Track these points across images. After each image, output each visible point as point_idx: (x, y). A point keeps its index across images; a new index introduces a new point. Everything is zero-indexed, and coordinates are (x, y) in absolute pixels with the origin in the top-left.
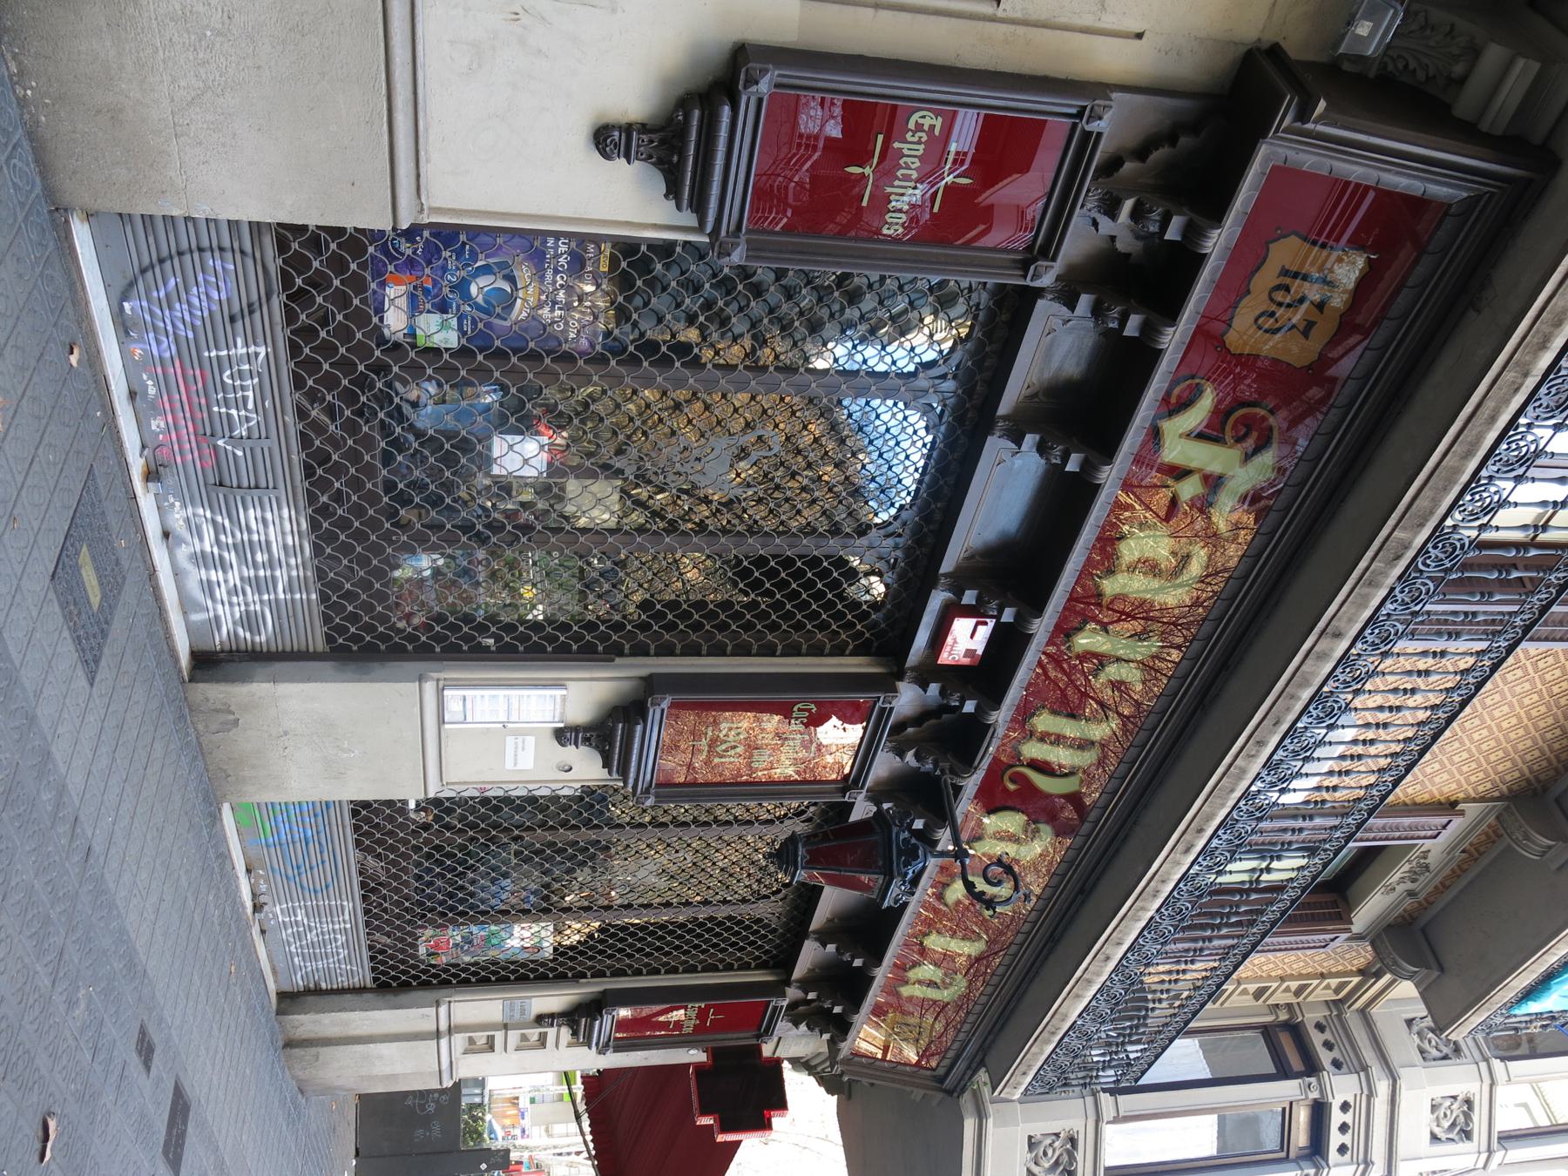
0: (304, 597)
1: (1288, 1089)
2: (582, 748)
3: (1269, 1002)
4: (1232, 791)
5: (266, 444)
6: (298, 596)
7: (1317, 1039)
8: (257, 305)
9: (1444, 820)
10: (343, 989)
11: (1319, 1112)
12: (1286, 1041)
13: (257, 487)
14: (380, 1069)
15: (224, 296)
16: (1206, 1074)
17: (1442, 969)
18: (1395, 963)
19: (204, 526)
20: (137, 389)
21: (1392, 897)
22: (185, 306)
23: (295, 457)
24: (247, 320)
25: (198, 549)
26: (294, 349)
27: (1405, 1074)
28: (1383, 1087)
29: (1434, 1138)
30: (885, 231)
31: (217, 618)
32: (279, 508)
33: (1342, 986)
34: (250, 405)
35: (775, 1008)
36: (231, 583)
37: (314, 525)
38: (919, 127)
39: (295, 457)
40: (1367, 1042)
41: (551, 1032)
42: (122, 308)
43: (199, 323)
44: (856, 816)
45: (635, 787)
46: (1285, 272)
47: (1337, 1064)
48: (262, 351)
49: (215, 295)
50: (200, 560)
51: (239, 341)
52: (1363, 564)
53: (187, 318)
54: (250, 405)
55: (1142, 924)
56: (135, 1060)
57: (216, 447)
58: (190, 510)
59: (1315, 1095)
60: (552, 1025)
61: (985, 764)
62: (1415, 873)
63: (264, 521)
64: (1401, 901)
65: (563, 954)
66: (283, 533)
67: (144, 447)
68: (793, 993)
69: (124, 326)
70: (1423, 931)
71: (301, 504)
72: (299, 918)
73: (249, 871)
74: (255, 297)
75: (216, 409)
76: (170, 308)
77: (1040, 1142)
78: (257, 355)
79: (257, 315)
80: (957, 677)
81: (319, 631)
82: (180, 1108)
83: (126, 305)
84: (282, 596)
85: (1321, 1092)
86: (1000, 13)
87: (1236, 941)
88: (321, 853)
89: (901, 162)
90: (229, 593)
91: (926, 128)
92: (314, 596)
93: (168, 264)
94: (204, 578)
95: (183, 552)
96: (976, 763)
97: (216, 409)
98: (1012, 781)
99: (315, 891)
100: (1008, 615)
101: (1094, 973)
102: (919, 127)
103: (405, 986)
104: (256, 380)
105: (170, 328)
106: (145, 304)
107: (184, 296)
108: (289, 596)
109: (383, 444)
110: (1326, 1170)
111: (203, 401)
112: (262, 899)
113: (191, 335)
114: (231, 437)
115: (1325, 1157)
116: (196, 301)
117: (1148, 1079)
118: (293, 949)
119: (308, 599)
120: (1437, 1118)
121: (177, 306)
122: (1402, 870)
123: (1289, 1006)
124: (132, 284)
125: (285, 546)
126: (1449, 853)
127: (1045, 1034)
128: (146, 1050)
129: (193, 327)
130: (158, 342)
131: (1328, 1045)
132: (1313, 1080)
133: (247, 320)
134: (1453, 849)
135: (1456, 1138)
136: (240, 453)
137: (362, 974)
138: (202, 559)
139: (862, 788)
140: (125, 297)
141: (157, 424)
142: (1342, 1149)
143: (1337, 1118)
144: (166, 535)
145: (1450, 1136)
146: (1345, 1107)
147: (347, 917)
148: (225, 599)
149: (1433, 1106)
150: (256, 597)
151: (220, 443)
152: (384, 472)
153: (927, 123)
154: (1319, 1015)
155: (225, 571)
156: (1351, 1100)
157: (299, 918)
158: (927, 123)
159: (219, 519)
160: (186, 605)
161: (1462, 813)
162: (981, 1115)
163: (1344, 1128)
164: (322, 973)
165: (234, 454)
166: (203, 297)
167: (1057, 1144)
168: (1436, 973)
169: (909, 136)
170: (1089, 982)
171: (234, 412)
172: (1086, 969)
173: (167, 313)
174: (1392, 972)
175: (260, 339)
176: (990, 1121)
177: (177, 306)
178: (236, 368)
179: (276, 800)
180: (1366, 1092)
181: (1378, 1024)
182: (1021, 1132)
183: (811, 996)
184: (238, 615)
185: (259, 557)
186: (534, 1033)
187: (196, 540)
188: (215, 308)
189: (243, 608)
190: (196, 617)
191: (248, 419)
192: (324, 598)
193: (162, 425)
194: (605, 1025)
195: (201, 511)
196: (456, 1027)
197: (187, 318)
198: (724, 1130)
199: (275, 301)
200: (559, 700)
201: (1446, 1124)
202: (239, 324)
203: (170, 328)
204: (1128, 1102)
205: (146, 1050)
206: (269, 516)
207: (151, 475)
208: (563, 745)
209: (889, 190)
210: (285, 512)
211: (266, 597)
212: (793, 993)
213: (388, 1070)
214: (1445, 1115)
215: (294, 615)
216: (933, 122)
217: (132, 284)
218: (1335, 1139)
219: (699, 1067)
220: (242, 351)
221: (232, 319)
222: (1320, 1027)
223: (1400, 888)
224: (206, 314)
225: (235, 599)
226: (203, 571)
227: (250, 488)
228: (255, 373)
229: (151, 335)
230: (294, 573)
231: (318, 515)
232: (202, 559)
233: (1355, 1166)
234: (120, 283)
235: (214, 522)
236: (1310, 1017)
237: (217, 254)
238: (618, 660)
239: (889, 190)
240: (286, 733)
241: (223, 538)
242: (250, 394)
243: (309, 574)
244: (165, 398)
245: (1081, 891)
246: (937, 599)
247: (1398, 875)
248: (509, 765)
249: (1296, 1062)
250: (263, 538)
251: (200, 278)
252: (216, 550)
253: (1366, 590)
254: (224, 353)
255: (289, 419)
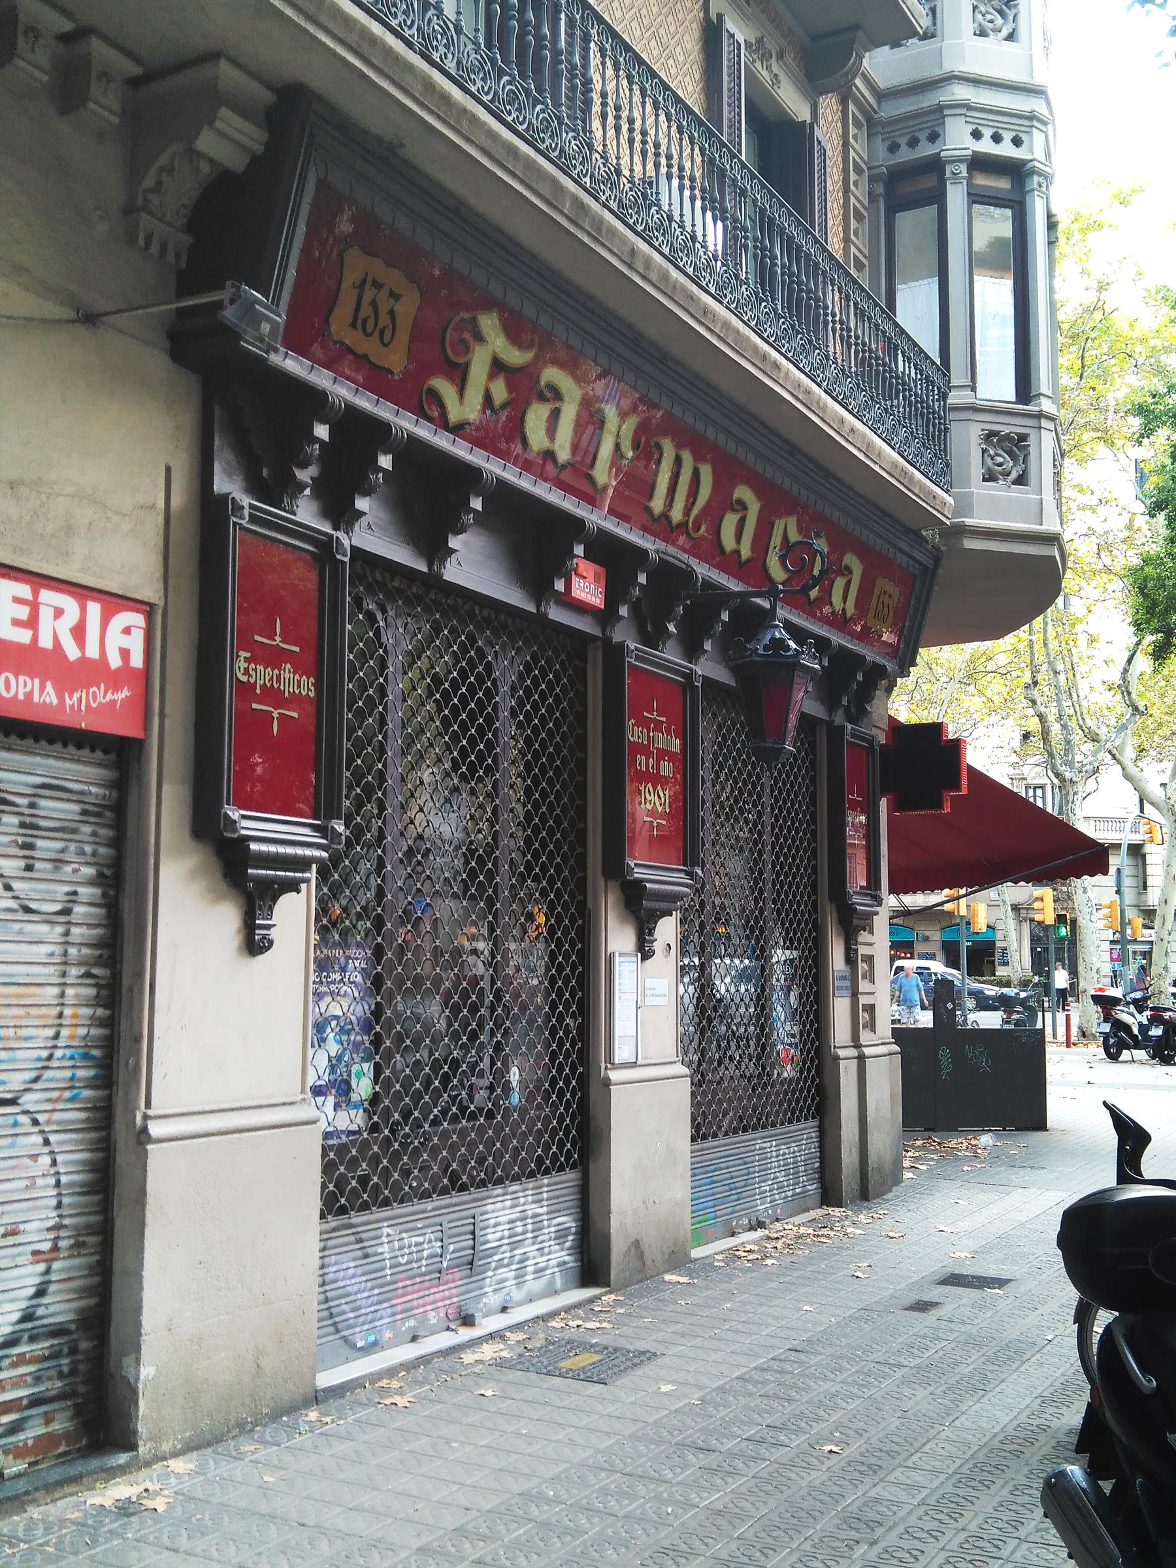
0: (545, 1189)
1: (956, 196)
2: (656, 936)
3: (866, 203)
4: (738, 332)
5: (446, 1226)
6: (545, 1195)
7: (905, 155)
8: (358, 1236)
9: (725, 35)
10: (820, 1147)
11: (979, 163)
12: (905, 188)
13: (473, 1233)
14: (886, 1111)
15: (352, 1264)
16: (933, 284)
17: (856, 27)
18: (846, 74)
19: (498, 1277)
20: (410, 1336)
21: (783, 78)
22: (359, 1296)
23: (455, 1200)
24: (366, 1244)
25: (513, 1282)
26: (386, 1203)
27: (951, 65)
28: (961, 92)
29: (1011, 37)
30: (312, 694)
31: (559, 1265)
32: (486, 1213)
33: (858, 125)
34: (420, 1239)
35: (853, 735)
36: (536, 1253)
37: (500, 1181)
38: (246, 671)
39: (455, 1200)
40: (914, 98)
41: (862, 950)
42: (361, 1348)
43: (369, 1285)
44: (721, 674)
45: (686, 885)
46: (353, 325)
47: (934, 137)
48: (386, 1231)
49: (351, 1271)
50: (521, 1280)
51: (380, 1250)
52: (586, 239)
53: (366, 1294)
54: (420, 1239)
55: (829, 399)
56: (934, 1314)
57: (448, 1268)
58: (487, 1289)
59: (963, 169)
60: (857, 950)
61: (684, 557)
62: (763, 55)
63: (495, 1225)
64: (788, 67)
65: (792, 943)
66: (504, 1209)
67: (448, 1329)
68: (839, 718)
69: (372, 1348)
70: (814, 38)
71: (485, 1194)
72: (767, 1188)
73: (733, 1234)
74: (352, 1238)
75: (423, 1269)
76: (359, 1308)
77: (989, 469)
78: (388, 1235)
79: (364, 1236)
80: (615, 591)
81: (556, 1177)
82: (955, 1280)
83: (359, 1345)
84: (545, 1209)
85: (961, 161)
86: (161, 603)
87: (852, 303)
88: (721, 1169)
89: (268, 685)
90: (542, 1255)
91: (246, 665)
92: (546, 1181)
93: (334, 1310)
94: (532, 1277)
95: (517, 1295)
96: (684, 566)
97: (423, 1269)
98: (699, 529)
99: (749, 1174)
100: (579, 550)
101: (863, 442)
102: (246, 671)
103: (820, 1089)
104: (404, 1235)
105: (372, 1309)
106: (357, 1329)
107: (352, 1298)
108: (545, 1203)
109: (445, 1124)
110: (1037, 164)
111: (418, 1280)
112: (754, 1223)
113: (376, 1291)
114: (441, 1256)
115: (1024, 163)
116: (356, 1288)
117: (930, 345)
118: (790, 1193)
119: (548, 1185)
120: (993, 30)
121: (359, 1303)
122: (760, 68)
123: (871, 180)
124: (345, 1339)
125: (513, 1207)
126: (749, 19)
127: (905, 482)
128: (922, 1306)
129: (372, 1289)
130: (381, 1318)
131: (913, 143)
132: (949, 169)
133: (366, 1244)
134: (745, 15)
135: (1014, 11)
136: (452, 1248)
137: (807, 1130)
138: (520, 1276)
139: (691, 670)
140: (353, 1346)
141: (433, 1318)
142: (1017, 142)
143: (986, 146)
144: (504, 1309)
145: (1011, 18)
146: (977, 135)
147: (768, 1144)
148: (546, 1258)
149: (980, 35)
150: (546, 1231)
151: (445, 1264)
152: (445, 1124)
153: (243, 665)
154: (881, 147)
155: (528, 1259)
156: (971, 128)
157: (767, 1188)
158: (243, 665)
159: (493, 1265)
160: (551, 1292)
161: (720, 17)
162: (962, 531)
163: (997, 138)
164: (808, 1167)
165: (453, 1252)
166: (353, 1281)
167: (992, 452)
168: (860, 34)
169: (252, 680)
170: (870, 445)
171: (425, 1253)
172: (859, 449)
173: (363, 1311)
174: (854, 78)
175: (378, 1233)
176: (969, 521)
177: (359, 1303)
178: (397, 1253)
179: (689, 1209)
180: (964, 111)
181: (895, 82)
182: (981, 490)
183: (845, 702)
184: (557, 1247)
185: (519, 1230)
186: (862, 967)
187: (507, 1284)
188: (359, 1271)
189: (552, 1243)
190: (558, 1284)
191: (430, 1241)
192: (547, 1172)
193: (433, 1313)
194: (860, 902)
195: (488, 1280)
196: (853, 1041)
197: (366, 1294)
198: (957, 787)
199: (354, 1221)
200: (622, 959)
201: (999, 21)
202: (370, 1250)
203: (372, 1309)
204: (958, 375)
205: (922, 1306)
206: (492, 1222)
207: (467, 1321)
208: (654, 952)
209: (287, 694)
210: (490, 1207)
211: (545, 1223)
212: (839, 718)
213: (887, 1103)
214: (991, 21)
215: (558, 1197)
216: (242, 659)
217: (345, 1339)
218: (1006, 149)
219: (892, 808)
220: (386, 1248)
221: (366, 1256)
222: (893, 148)
223: (775, 68)
224: (364, 1278)
225: (546, 1250)
226: (528, 1278)
227: (474, 1239)
228: (400, 1236)
229: (377, 1324)
230: (530, 1198)
231: (492, 1180)
232: (520, 1276)
233: (1035, 130)
234: (346, 1350)
235: (496, 1269)
236: (884, 159)
237: (325, 1270)
238: (590, 904)
239: (287, 694)
240: (645, 1202)
241: (506, 1261)
242: (414, 1240)
243: (531, 1185)
244: (416, 1311)
245: (792, 454)
246: (555, 614)
247: (765, 73)
248: (663, 1001)
249: (930, 182)
250: (507, 1227)
251: (341, 1284)
252: (514, 1267)
253: (604, 231)
254: (388, 1263)
255: (430, 1206)
